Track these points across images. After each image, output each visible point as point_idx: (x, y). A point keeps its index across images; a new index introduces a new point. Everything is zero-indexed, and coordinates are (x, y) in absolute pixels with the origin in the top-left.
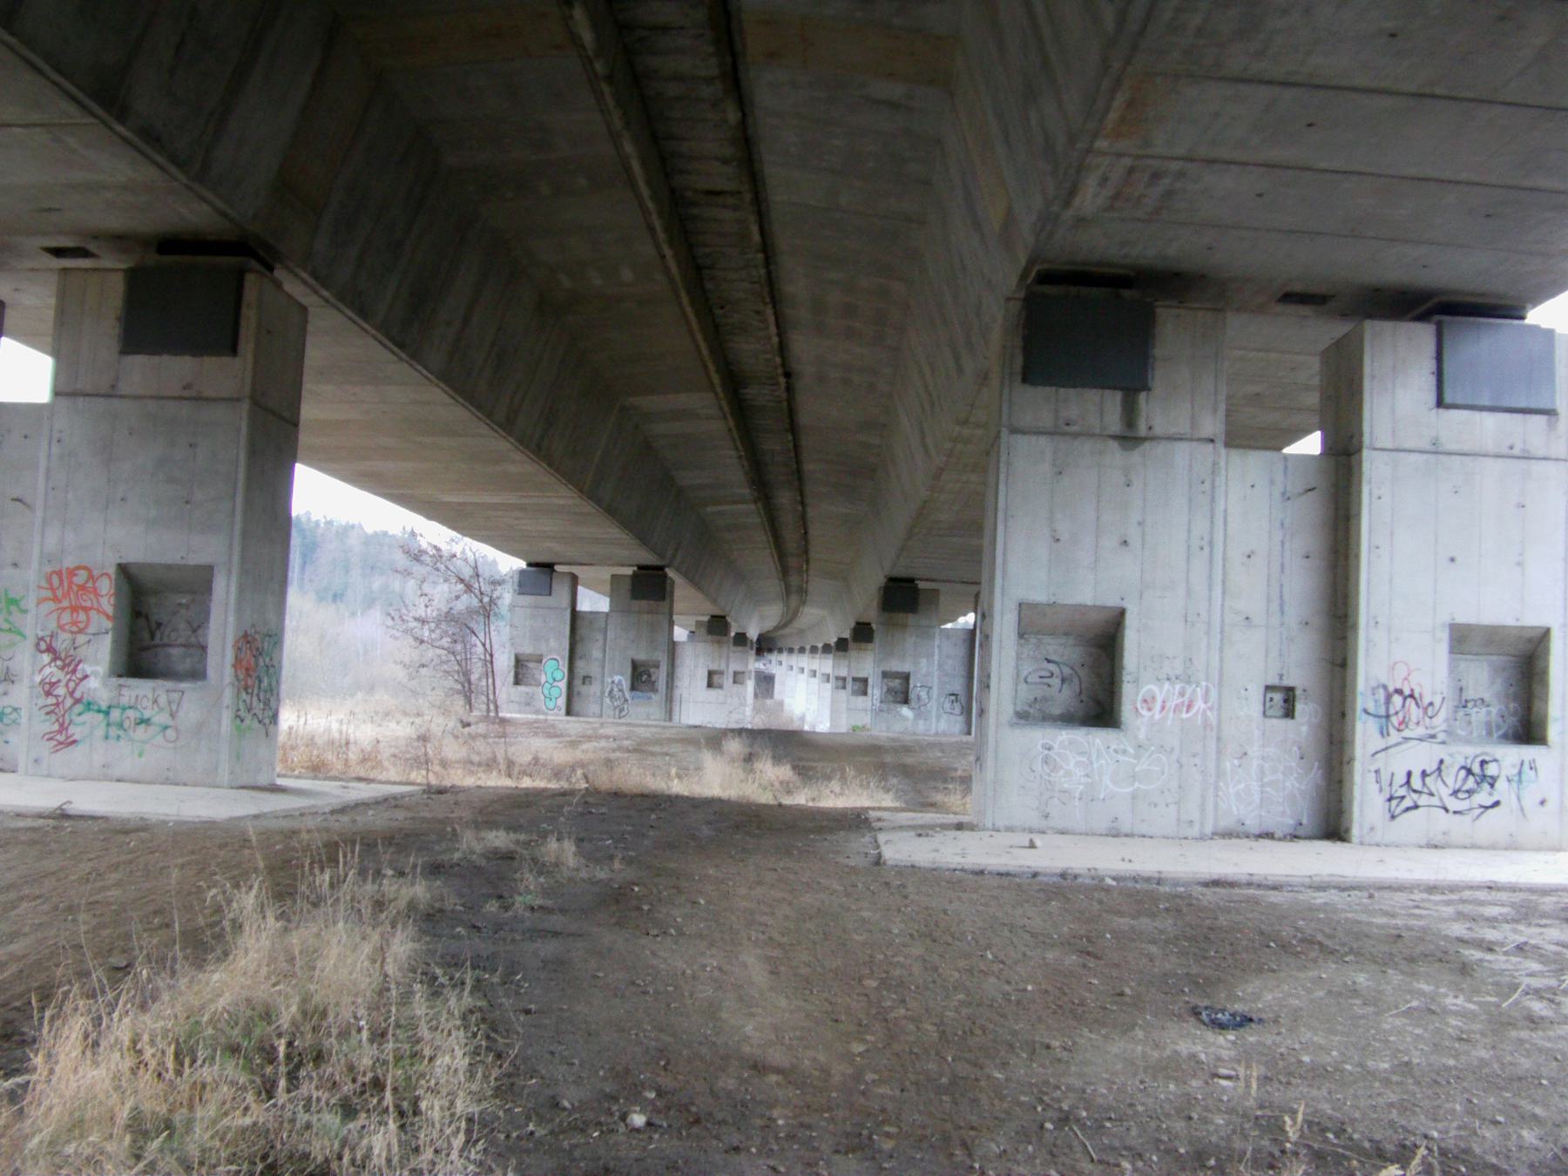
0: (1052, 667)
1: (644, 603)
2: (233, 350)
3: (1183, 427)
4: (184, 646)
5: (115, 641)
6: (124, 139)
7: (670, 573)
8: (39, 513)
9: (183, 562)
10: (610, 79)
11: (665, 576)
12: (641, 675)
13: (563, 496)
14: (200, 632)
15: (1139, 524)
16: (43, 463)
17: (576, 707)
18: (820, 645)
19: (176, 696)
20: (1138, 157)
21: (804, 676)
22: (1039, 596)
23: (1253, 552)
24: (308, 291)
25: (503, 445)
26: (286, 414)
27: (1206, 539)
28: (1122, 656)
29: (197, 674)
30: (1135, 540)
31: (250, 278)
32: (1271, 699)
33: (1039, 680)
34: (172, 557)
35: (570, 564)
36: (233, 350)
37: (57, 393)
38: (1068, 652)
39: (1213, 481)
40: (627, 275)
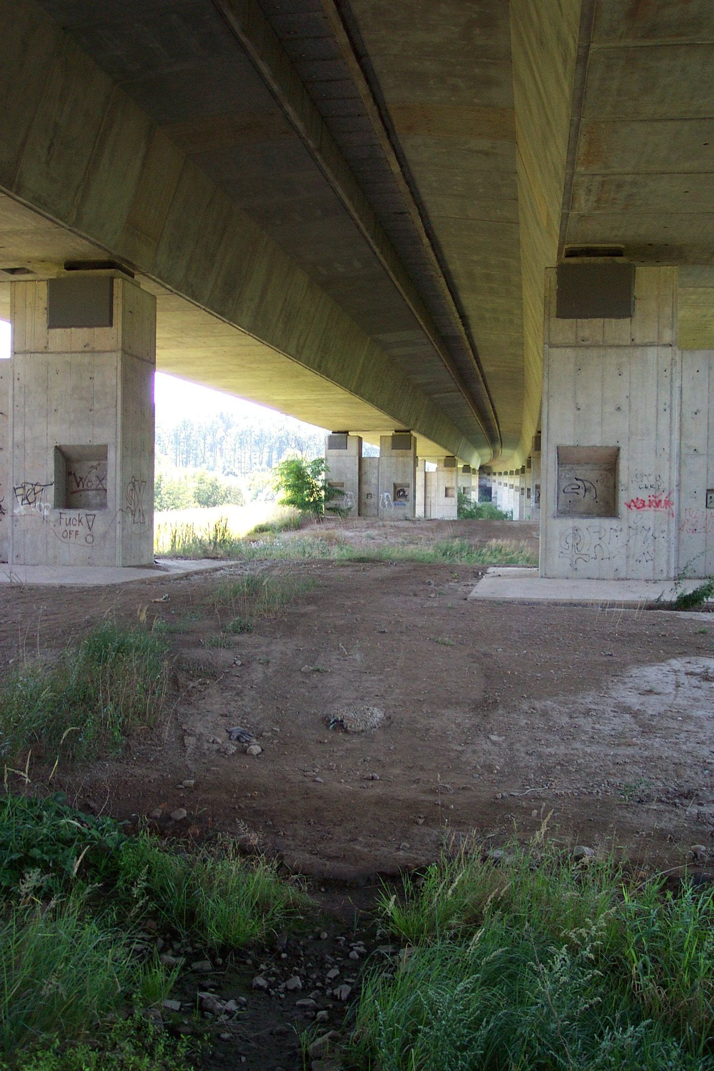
0: (579, 483)
1: (399, 451)
2: (111, 325)
3: (652, 337)
4: (97, 490)
5: (56, 489)
6: (25, 205)
7: (414, 434)
8: (10, 420)
9: (91, 444)
10: (319, 150)
11: (411, 435)
12: (399, 492)
13: (340, 394)
14: (103, 482)
15: (627, 397)
16: (11, 393)
17: (363, 511)
18: (503, 472)
19: (91, 518)
20: (604, 176)
21: (507, 488)
22: (569, 442)
23: (698, 411)
24: (159, 286)
25: (297, 367)
26: (147, 358)
27: (668, 403)
28: (619, 476)
29: (103, 505)
30: (625, 408)
31: (118, 282)
32: (711, 497)
33: (571, 490)
34: (85, 441)
35: (357, 431)
36: (111, 325)
37: (15, 353)
38: (591, 474)
39: (672, 369)
40: (357, 264)
